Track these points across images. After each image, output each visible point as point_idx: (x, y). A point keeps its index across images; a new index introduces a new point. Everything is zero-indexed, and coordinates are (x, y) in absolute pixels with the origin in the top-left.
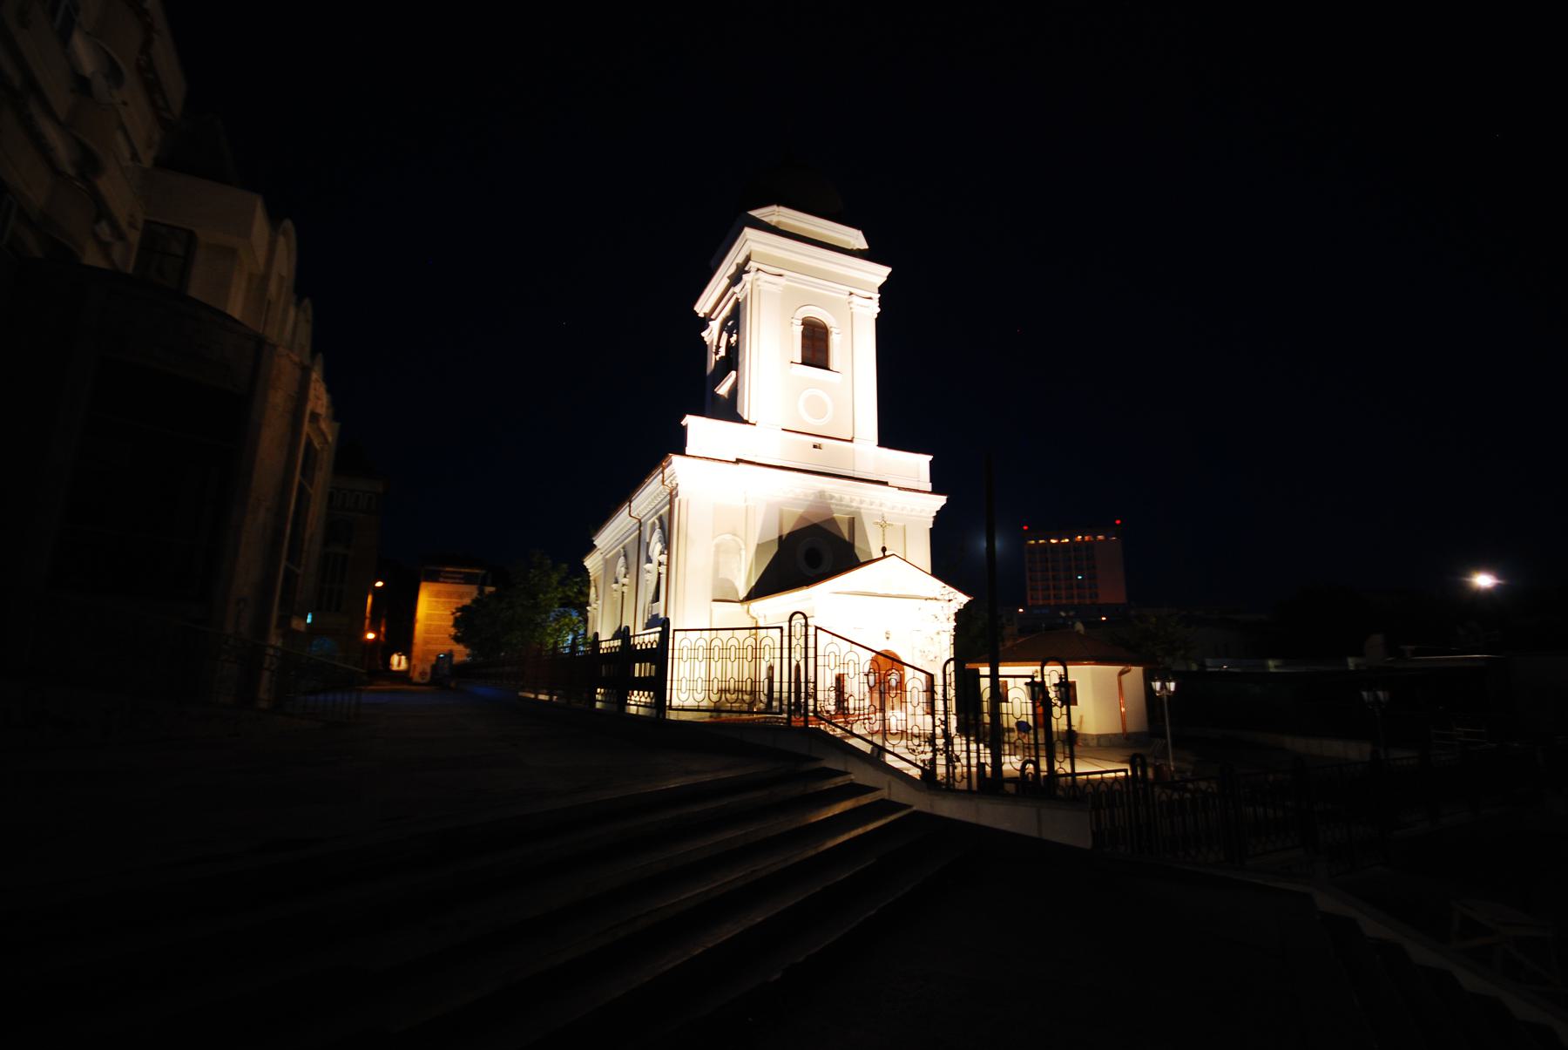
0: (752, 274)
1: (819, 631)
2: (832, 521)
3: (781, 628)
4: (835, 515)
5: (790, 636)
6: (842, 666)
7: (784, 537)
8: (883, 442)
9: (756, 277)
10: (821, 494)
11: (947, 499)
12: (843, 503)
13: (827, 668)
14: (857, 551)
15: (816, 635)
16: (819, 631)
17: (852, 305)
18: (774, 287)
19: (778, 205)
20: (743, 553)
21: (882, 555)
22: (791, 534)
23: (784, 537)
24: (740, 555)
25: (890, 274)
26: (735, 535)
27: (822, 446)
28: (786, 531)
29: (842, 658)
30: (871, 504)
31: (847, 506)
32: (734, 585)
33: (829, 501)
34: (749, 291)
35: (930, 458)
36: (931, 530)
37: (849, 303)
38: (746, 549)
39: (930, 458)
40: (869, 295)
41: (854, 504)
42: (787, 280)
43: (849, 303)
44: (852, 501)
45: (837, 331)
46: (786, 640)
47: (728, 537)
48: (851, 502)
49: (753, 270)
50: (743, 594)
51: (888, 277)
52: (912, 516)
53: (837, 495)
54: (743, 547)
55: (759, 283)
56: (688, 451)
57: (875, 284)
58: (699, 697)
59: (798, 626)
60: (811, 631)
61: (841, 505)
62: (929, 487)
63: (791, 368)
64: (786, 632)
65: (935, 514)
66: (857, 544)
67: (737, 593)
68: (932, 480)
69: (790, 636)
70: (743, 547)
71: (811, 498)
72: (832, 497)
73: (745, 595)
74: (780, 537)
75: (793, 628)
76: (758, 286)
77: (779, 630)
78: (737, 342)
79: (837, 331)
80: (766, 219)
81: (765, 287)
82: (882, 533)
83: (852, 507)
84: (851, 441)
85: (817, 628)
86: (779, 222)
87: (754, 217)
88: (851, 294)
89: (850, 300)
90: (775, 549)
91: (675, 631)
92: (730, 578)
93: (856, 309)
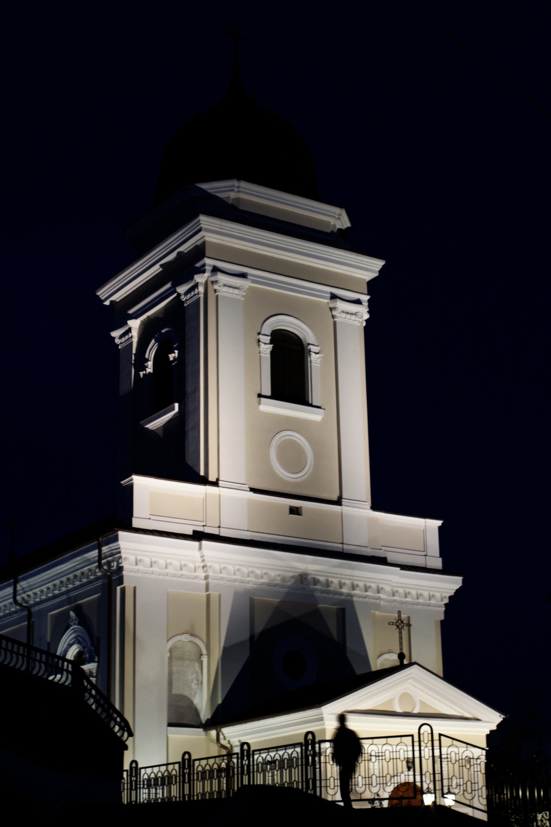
0: (207, 275)
1: (442, 737)
2: (316, 613)
3: (412, 736)
4: (320, 606)
5: (420, 741)
6: (461, 761)
7: (256, 638)
8: (375, 507)
9: (213, 279)
10: (303, 578)
11: (463, 580)
12: (331, 589)
13: (449, 763)
14: (349, 655)
15: (440, 740)
16: (442, 737)
17: (334, 313)
18: (236, 292)
19: (239, 179)
20: (205, 659)
21: (398, 663)
22: (264, 633)
23: (256, 638)
24: (201, 663)
25: (383, 266)
26: (192, 635)
27: (304, 512)
28: (258, 629)
29: (460, 754)
30: (366, 589)
31: (335, 593)
32: (192, 703)
33: (312, 587)
34: (202, 296)
35: (439, 523)
36: (443, 624)
37: (331, 309)
38: (209, 654)
39: (439, 523)
40: (355, 296)
41: (345, 590)
42: (253, 281)
43: (331, 309)
44: (341, 585)
45: (316, 349)
46: (416, 744)
47: (185, 638)
48: (341, 588)
49: (208, 268)
50: (205, 714)
51: (380, 272)
52: (418, 604)
53: (322, 579)
54: (204, 651)
55: (216, 287)
56: (136, 523)
57: (365, 280)
58: (360, 789)
59: (426, 734)
60: (436, 737)
61: (328, 592)
62: (438, 563)
63: (260, 403)
64: (416, 739)
65: (446, 601)
66: (350, 645)
67: (196, 712)
68: (442, 555)
69: (420, 741)
70: (204, 651)
71: (289, 584)
72: (316, 582)
73: (209, 716)
74: (252, 637)
75: (422, 736)
76: (215, 291)
77: (410, 738)
78: (181, 358)
79: (316, 349)
80: (221, 195)
81: (223, 292)
82: (398, 635)
83: (341, 594)
84: (338, 502)
85: (440, 735)
86: (238, 199)
87: (204, 191)
88: (334, 297)
89: (332, 305)
90: (246, 654)
91: (254, 751)
92: (186, 693)
93: (341, 318)
